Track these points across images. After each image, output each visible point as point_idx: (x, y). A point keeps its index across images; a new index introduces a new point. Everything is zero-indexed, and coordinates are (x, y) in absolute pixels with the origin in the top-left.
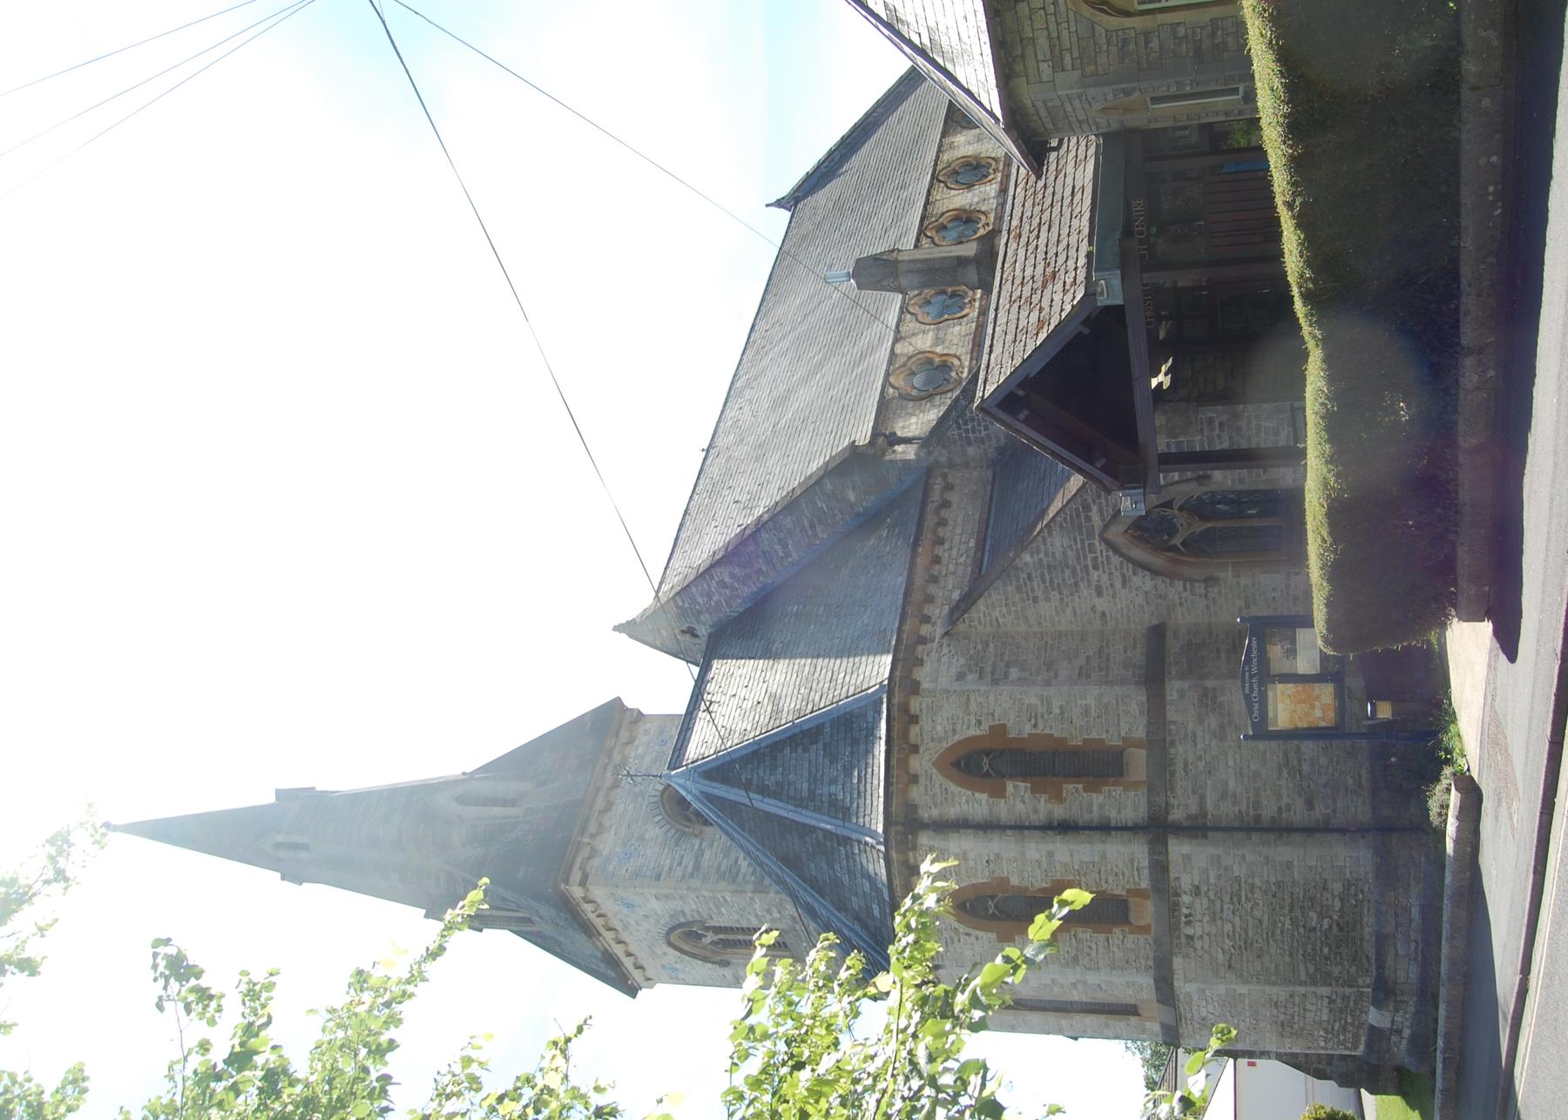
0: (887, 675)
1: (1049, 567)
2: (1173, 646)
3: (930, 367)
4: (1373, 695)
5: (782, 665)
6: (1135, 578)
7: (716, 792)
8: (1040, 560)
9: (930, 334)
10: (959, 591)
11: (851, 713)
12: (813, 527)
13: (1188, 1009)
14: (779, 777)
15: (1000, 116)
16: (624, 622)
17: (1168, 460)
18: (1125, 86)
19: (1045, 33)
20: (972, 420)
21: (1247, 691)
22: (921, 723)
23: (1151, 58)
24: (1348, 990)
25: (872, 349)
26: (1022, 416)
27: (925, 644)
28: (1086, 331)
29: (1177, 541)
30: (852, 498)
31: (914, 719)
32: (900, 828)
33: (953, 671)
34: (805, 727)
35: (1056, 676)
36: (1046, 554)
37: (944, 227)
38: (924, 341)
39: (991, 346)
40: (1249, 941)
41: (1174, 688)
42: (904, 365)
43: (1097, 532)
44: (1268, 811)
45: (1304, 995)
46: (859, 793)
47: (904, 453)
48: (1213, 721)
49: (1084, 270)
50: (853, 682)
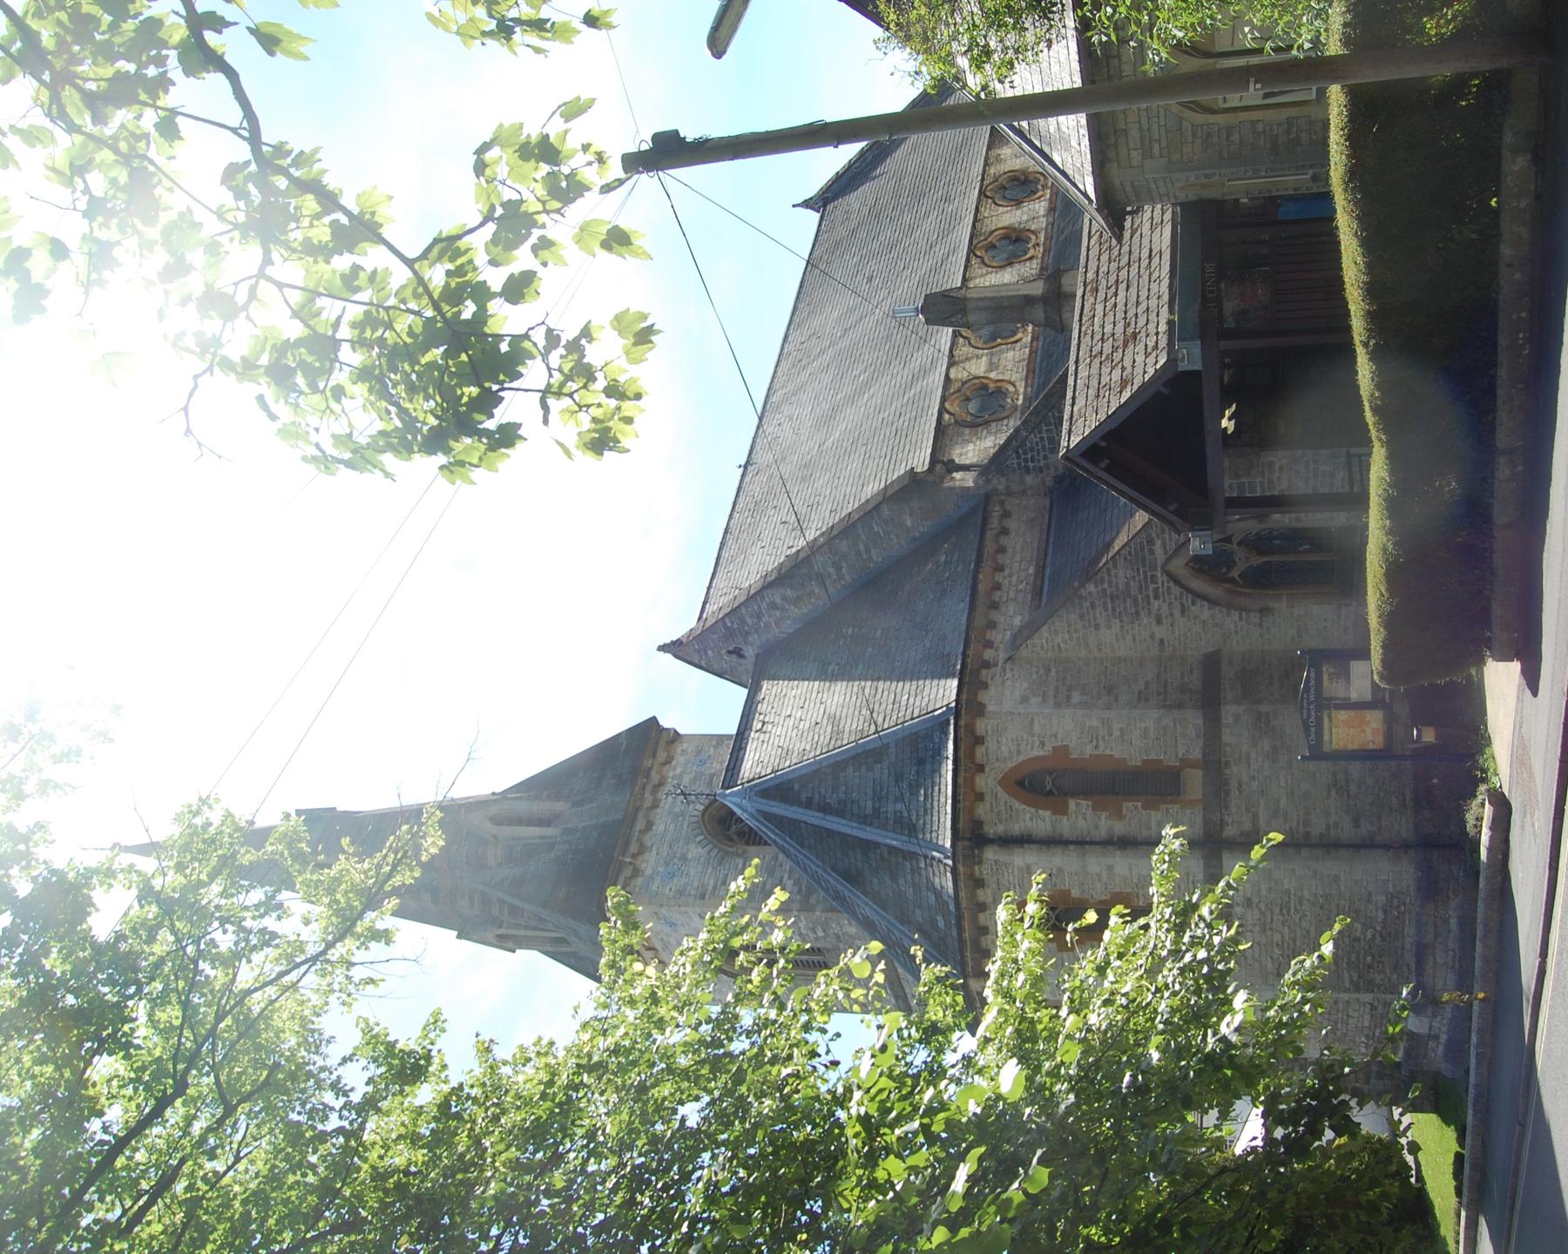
0: (953, 697)
3: (984, 392)
4: (1419, 720)
5: (840, 687)
6: (1193, 608)
7: (775, 810)
8: (1104, 591)
9: (984, 359)
11: (916, 734)
12: (868, 550)
14: (842, 796)
15: (1092, 196)
16: (668, 641)
17: (1235, 503)
19: (1137, 126)
20: (1032, 450)
21: (1305, 715)
25: (924, 372)
26: (1103, 465)
28: (1166, 391)
29: (1235, 573)
30: (909, 524)
31: (980, 740)
32: (967, 843)
33: (1018, 694)
34: (867, 748)
35: (1116, 700)
36: (1110, 583)
37: (993, 246)
38: (978, 367)
39: (1074, 398)
41: (1229, 712)
42: (959, 391)
43: (1159, 564)
44: (1317, 829)
45: (1348, 1002)
46: (925, 810)
47: (962, 480)
48: (1266, 744)
49: (1166, 336)
50: (917, 704)
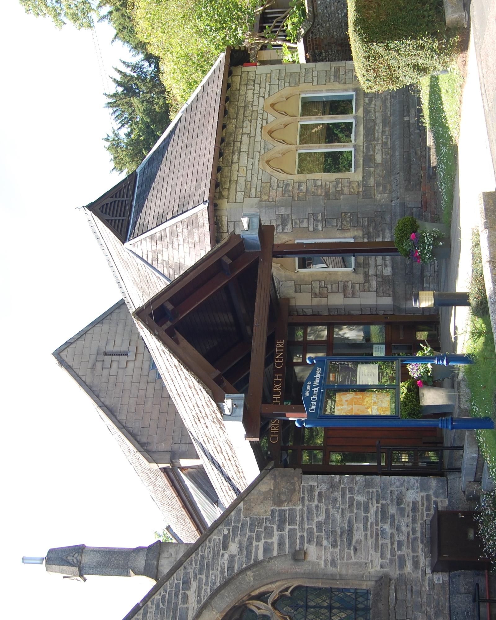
19: (244, 178)
23: (300, 196)
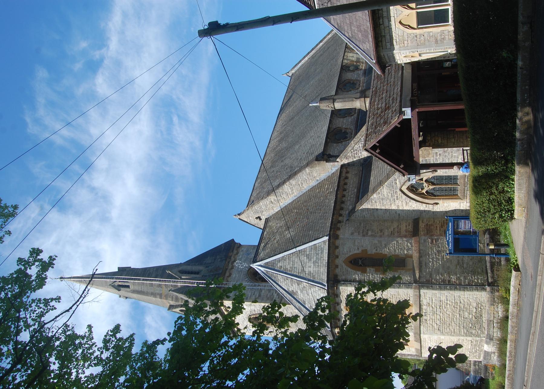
1: (382, 199)
2: (422, 225)
10: (351, 206)
13: (425, 344)
18: (413, 50)
19: (389, 34)
22: (339, 248)
24: (477, 338)
26: (402, 166)
27: (340, 223)
28: (399, 126)
31: (337, 247)
35: (383, 234)
40: (445, 321)
